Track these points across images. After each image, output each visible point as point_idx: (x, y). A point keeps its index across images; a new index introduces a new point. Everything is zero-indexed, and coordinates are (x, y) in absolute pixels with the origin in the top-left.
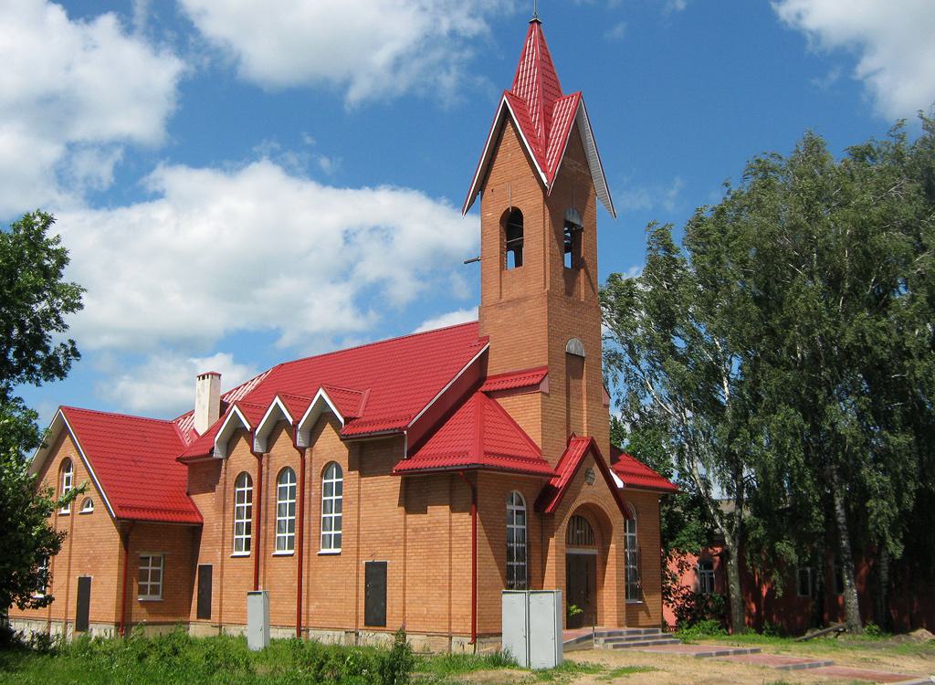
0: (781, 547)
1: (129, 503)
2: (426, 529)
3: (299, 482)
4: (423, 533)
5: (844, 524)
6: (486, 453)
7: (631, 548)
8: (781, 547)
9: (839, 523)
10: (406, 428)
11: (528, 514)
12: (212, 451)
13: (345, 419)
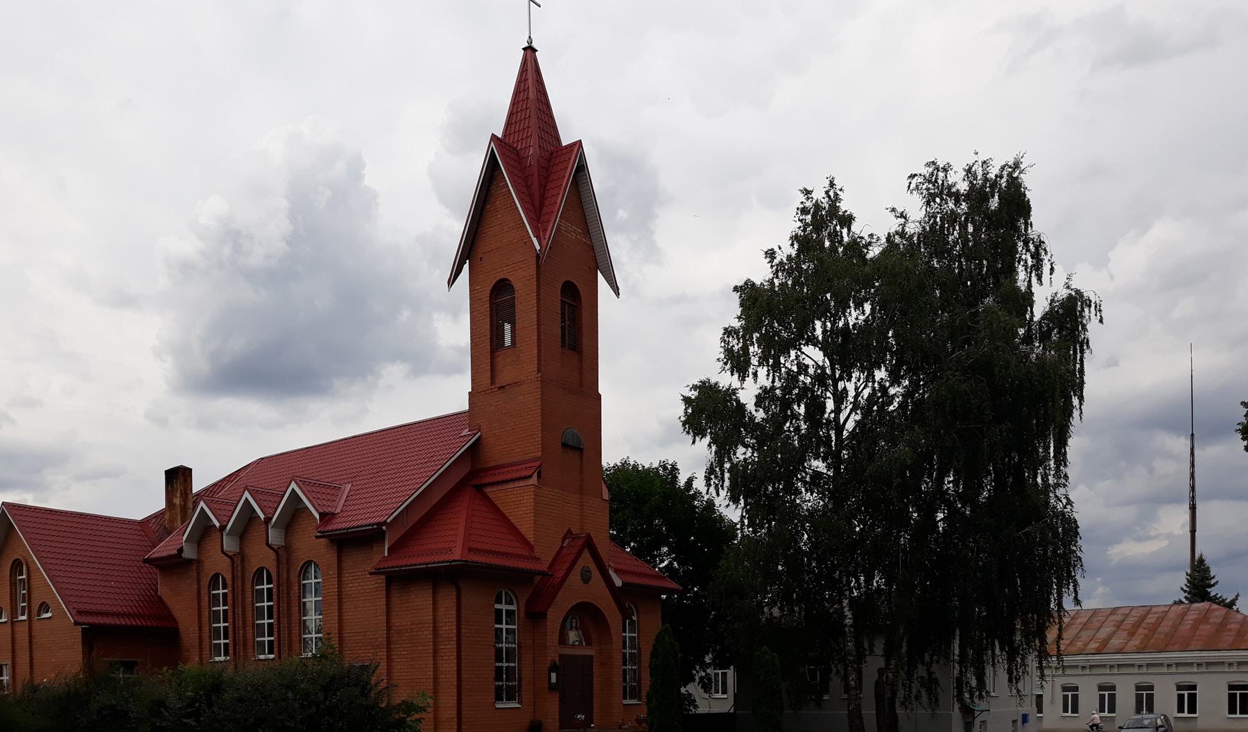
0: (789, 414)
1: (88, 607)
2: (409, 631)
3: (276, 584)
4: (406, 634)
5: (851, 626)
6: (470, 550)
7: (631, 648)
8: (789, 414)
9: (846, 625)
10: (385, 523)
11: (518, 614)
12: (181, 550)
13: (320, 514)
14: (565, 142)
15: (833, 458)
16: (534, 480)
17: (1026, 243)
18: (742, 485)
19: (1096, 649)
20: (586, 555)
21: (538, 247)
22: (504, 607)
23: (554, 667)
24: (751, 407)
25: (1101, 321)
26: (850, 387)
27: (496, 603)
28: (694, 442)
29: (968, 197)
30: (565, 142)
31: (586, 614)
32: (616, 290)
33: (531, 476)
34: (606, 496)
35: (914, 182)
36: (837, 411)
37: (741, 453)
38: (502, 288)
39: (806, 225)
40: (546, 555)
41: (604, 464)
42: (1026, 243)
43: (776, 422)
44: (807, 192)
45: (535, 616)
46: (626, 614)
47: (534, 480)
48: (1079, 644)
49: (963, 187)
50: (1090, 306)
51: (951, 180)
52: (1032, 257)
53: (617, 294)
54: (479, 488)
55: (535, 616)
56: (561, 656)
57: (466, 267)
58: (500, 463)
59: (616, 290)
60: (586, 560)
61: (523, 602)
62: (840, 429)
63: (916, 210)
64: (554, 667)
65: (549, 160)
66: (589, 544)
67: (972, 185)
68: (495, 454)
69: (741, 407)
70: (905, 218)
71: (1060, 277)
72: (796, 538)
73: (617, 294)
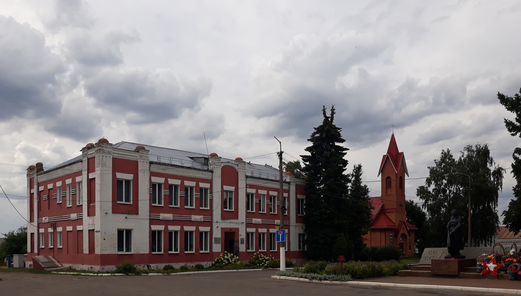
14: (400, 152)
16: (395, 212)
19: (518, 237)
20: (404, 224)
21: (397, 173)
22: (391, 234)
23: (399, 245)
24: (431, 192)
25: (506, 173)
27: (185, 205)
29: (476, 151)
30: (400, 152)
31: (403, 235)
33: (395, 212)
34: (406, 213)
35: (465, 148)
37: (430, 202)
38: (388, 178)
39: (443, 156)
40: (397, 225)
41: (312, 145)
43: (436, 195)
44: (443, 150)
45: (396, 236)
46: (410, 235)
47: (395, 212)
49: (475, 149)
50: (503, 170)
51: (472, 149)
52: (490, 161)
53: (408, 177)
54: (384, 213)
55: (396, 236)
56: (400, 243)
57: (381, 173)
58: (387, 208)
60: (404, 226)
61: (394, 233)
62: (450, 196)
64: (399, 245)
66: (404, 223)
67: (477, 148)
68: (387, 207)
69: (430, 192)
70: (464, 154)
71: (496, 165)
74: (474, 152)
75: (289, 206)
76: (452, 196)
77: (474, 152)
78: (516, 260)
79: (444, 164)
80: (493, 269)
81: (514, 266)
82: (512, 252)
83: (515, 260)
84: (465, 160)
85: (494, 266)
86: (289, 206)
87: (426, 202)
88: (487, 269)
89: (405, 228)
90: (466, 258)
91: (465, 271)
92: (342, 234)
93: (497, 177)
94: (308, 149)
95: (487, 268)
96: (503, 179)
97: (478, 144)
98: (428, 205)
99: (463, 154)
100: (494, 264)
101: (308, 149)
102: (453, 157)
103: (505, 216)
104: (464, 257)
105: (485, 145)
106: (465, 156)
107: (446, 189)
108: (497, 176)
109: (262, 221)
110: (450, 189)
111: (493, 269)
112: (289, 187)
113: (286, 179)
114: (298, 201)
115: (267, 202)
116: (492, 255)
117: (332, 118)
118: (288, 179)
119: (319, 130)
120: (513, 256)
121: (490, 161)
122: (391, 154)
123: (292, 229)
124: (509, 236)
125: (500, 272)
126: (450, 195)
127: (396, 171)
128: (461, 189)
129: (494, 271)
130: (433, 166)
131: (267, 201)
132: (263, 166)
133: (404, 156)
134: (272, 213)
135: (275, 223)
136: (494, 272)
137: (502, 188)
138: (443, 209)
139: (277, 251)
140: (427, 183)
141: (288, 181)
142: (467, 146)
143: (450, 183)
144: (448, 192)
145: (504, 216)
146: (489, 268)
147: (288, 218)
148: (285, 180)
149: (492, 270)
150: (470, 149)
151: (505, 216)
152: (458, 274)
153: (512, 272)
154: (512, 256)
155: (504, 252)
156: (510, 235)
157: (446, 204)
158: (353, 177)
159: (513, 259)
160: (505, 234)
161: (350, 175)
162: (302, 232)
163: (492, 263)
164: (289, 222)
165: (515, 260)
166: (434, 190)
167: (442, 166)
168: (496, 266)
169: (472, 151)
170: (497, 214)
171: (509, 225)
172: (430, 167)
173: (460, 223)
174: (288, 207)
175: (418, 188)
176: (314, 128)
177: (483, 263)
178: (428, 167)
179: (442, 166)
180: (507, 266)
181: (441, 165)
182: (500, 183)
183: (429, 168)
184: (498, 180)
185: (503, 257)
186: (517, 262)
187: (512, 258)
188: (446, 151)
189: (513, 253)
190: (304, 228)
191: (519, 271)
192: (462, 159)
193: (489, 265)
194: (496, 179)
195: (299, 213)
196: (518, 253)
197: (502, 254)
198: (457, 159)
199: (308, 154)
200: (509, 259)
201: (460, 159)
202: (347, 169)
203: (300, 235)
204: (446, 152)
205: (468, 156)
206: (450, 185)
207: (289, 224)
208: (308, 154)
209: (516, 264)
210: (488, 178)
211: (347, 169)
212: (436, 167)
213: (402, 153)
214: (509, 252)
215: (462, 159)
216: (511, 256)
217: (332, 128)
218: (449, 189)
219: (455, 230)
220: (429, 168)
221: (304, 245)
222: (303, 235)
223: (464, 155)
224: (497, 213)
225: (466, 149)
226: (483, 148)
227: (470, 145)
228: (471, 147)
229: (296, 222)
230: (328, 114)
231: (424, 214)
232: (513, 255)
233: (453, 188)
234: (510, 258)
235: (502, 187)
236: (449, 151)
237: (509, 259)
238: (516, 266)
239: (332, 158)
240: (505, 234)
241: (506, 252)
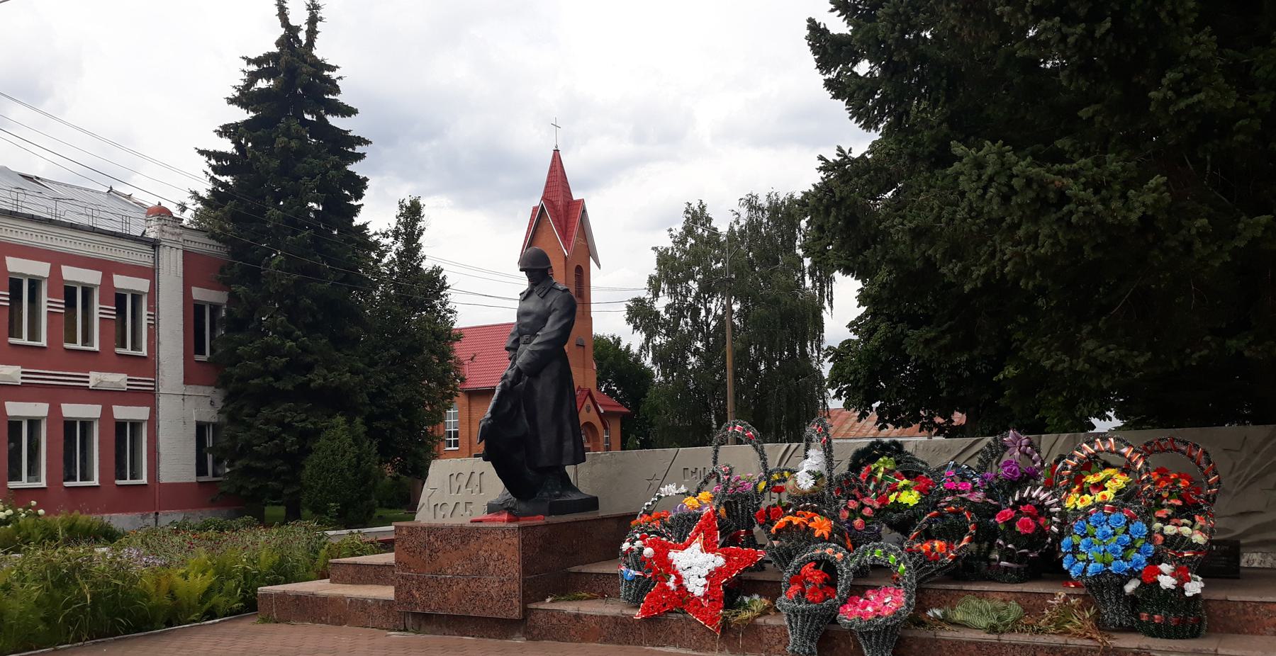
15: (705, 338)
17: (800, 230)
18: (659, 357)
20: (588, 398)
21: (567, 254)
24: (662, 313)
26: (713, 306)
28: (633, 333)
32: (599, 266)
34: (595, 368)
35: (742, 202)
36: (707, 317)
37: (658, 340)
39: (688, 219)
42: (800, 230)
44: (689, 204)
46: (606, 428)
48: (864, 431)
49: (766, 205)
51: (759, 202)
52: (803, 236)
53: (600, 268)
59: (599, 266)
60: (589, 401)
62: (708, 325)
63: (744, 213)
65: (568, 207)
67: (771, 203)
69: (658, 313)
70: (739, 216)
72: (686, 383)
73: (600, 268)
74: (763, 213)
75: (154, 325)
76: (714, 323)
77: (763, 213)
78: (826, 523)
79: (693, 242)
80: (704, 581)
81: (816, 567)
82: (809, 472)
83: (821, 526)
84: (742, 233)
85: (711, 566)
86: (154, 325)
87: (647, 340)
88: (671, 584)
89: (592, 407)
90: (604, 511)
91: (567, 587)
92: (340, 419)
93: (819, 279)
94: (226, 131)
95: (673, 578)
96: (834, 284)
97: (772, 190)
98: (654, 346)
99: (737, 216)
100: (708, 547)
101: (226, 131)
102: (714, 224)
103: (832, 363)
104: (592, 503)
105: (790, 194)
106: (743, 222)
107: (700, 306)
108: (821, 276)
109: (23, 373)
110: (708, 305)
111: (704, 581)
112: (156, 259)
113: (147, 230)
114: (195, 314)
115: (49, 307)
116: (704, 496)
117: (312, 33)
118: (152, 229)
119: (264, 65)
120: (815, 500)
121: (802, 238)
122: (552, 202)
123: (166, 406)
124: (855, 433)
125: (747, 600)
126: (709, 321)
127: (565, 251)
128: (736, 307)
129: (705, 596)
130: (665, 246)
131: (100, 308)
132: (104, 193)
133: (584, 211)
134: (128, 350)
135: (88, 382)
136: (706, 604)
137: (832, 307)
138: (692, 359)
139: (97, 484)
140: (649, 291)
141: (152, 236)
142: (747, 195)
143: (708, 289)
144: (703, 313)
145: (830, 361)
146: (679, 579)
147: (147, 365)
148: (144, 233)
149: (699, 592)
150: (754, 202)
151: (832, 363)
152: (526, 612)
153: (803, 606)
154: (804, 497)
155: (768, 474)
156: (858, 429)
157: (699, 344)
158: (396, 238)
159: (811, 520)
160: (847, 426)
161: (389, 232)
162: (209, 415)
163: (696, 546)
164: (154, 382)
165: (821, 526)
166: (668, 308)
167: (688, 245)
168: (720, 561)
169: (760, 209)
170: (821, 372)
171: (845, 389)
172: (659, 249)
173: (560, 319)
174: (148, 327)
175: (629, 303)
176: (243, 58)
177: (650, 545)
178: (653, 249)
179: (688, 245)
180: (785, 557)
181: (684, 245)
182: (828, 295)
183: (655, 249)
184: (822, 287)
185: (764, 506)
186: (831, 535)
187: (805, 509)
188: (695, 206)
189: (811, 483)
190: (219, 405)
191: (845, 602)
192: (736, 228)
193: (679, 558)
194: (818, 284)
195: (200, 349)
196: (839, 481)
197: (756, 486)
198: (723, 229)
199: (227, 146)
200: (786, 519)
201: (731, 228)
202: (363, 205)
203: (201, 428)
204: (696, 208)
205: (750, 222)
206: (707, 296)
207: (154, 386)
208: (227, 146)
209: (829, 551)
210: (798, 281)
211: (363, 205)
212: (673, 249)
213: (581, 202)
214: (792, 472)
215: (736, 228)
216: (801, 499)
217: (306, 62)
218: (706, 307)
219: (532, 352)
220: (655, 249)
221: (217, 462)
222: (217, 427)
223: (740, 221)
224: (822, 370)
225: (743, 204)
226: (784, 203)
227: (754, 194)
228: (757, 197)
229: (184, 384)
230: (299, 17)
231: (648, 374)
232: (812, 490)
233: (716, 305)
234: (794, 514)
235: (833, 305)
236: (703, 207)
237: (786, 519)
238: (828, 567)
239: (305, 162)
240: (847, 426)
241: (776, 476)
